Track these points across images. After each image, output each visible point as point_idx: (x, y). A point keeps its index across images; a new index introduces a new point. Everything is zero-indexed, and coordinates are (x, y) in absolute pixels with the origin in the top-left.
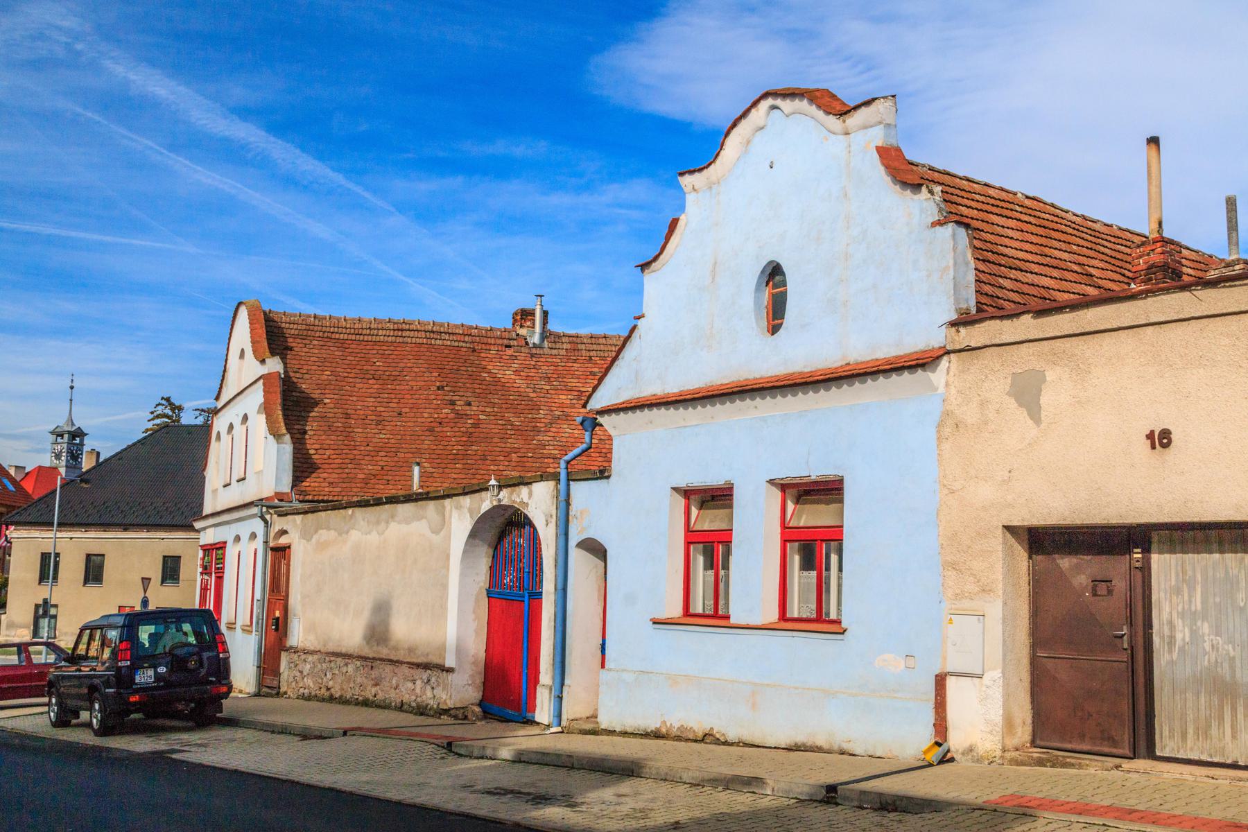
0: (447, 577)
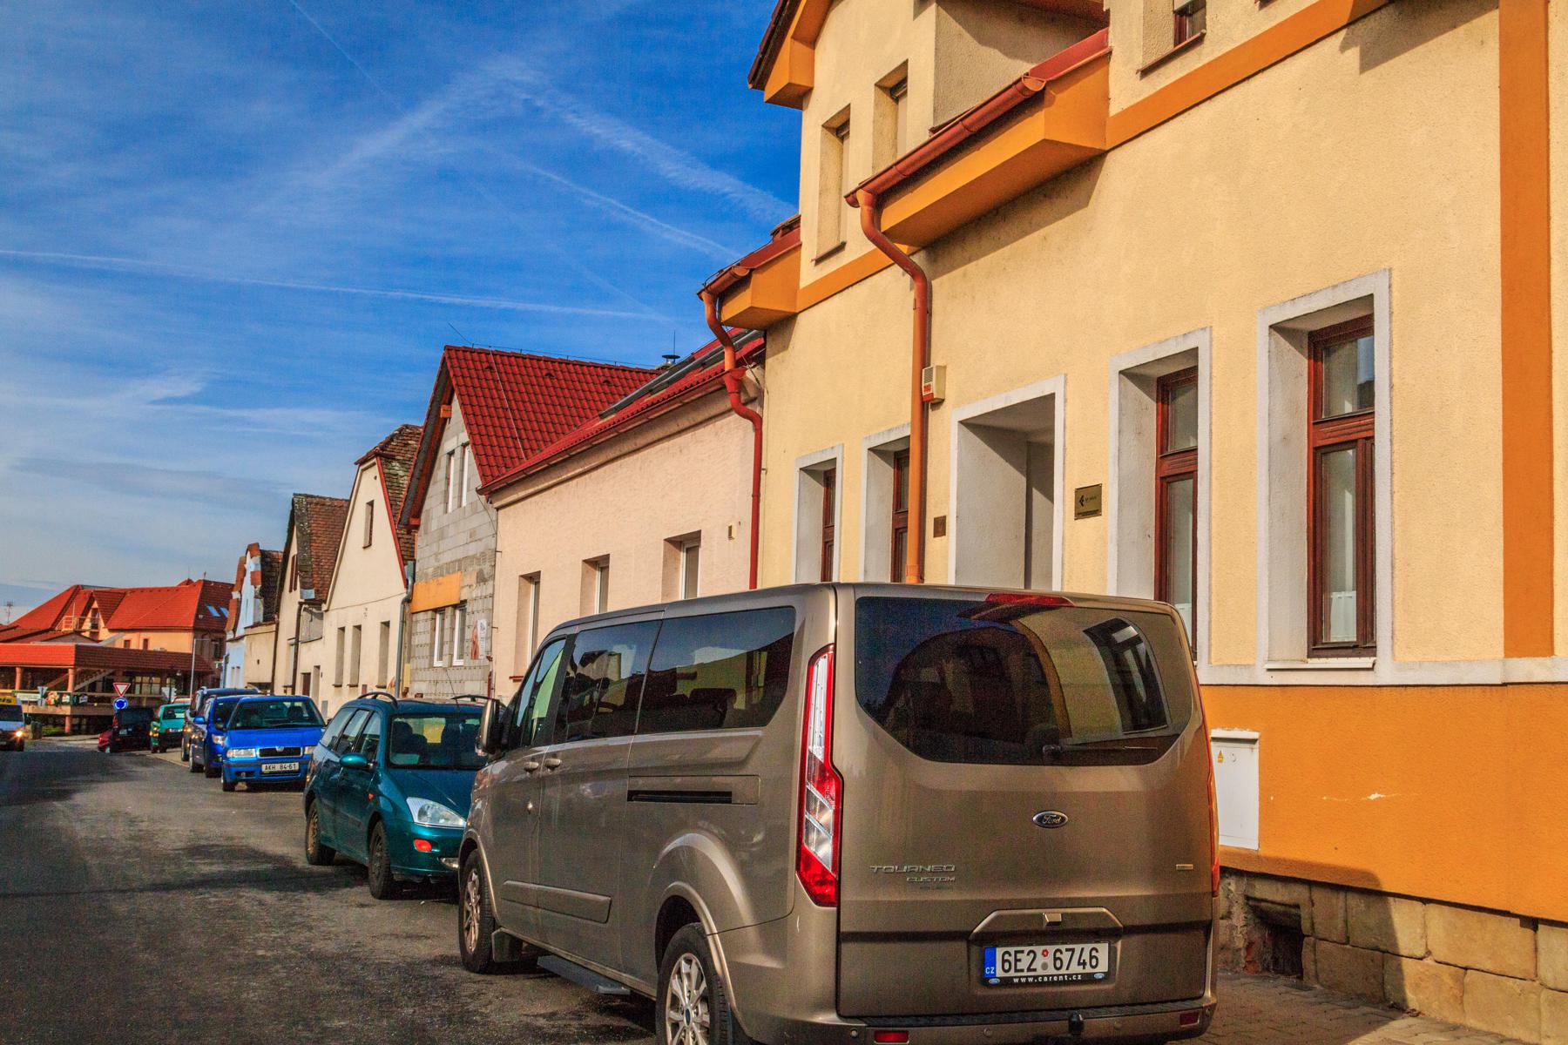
0: (1006, 916)
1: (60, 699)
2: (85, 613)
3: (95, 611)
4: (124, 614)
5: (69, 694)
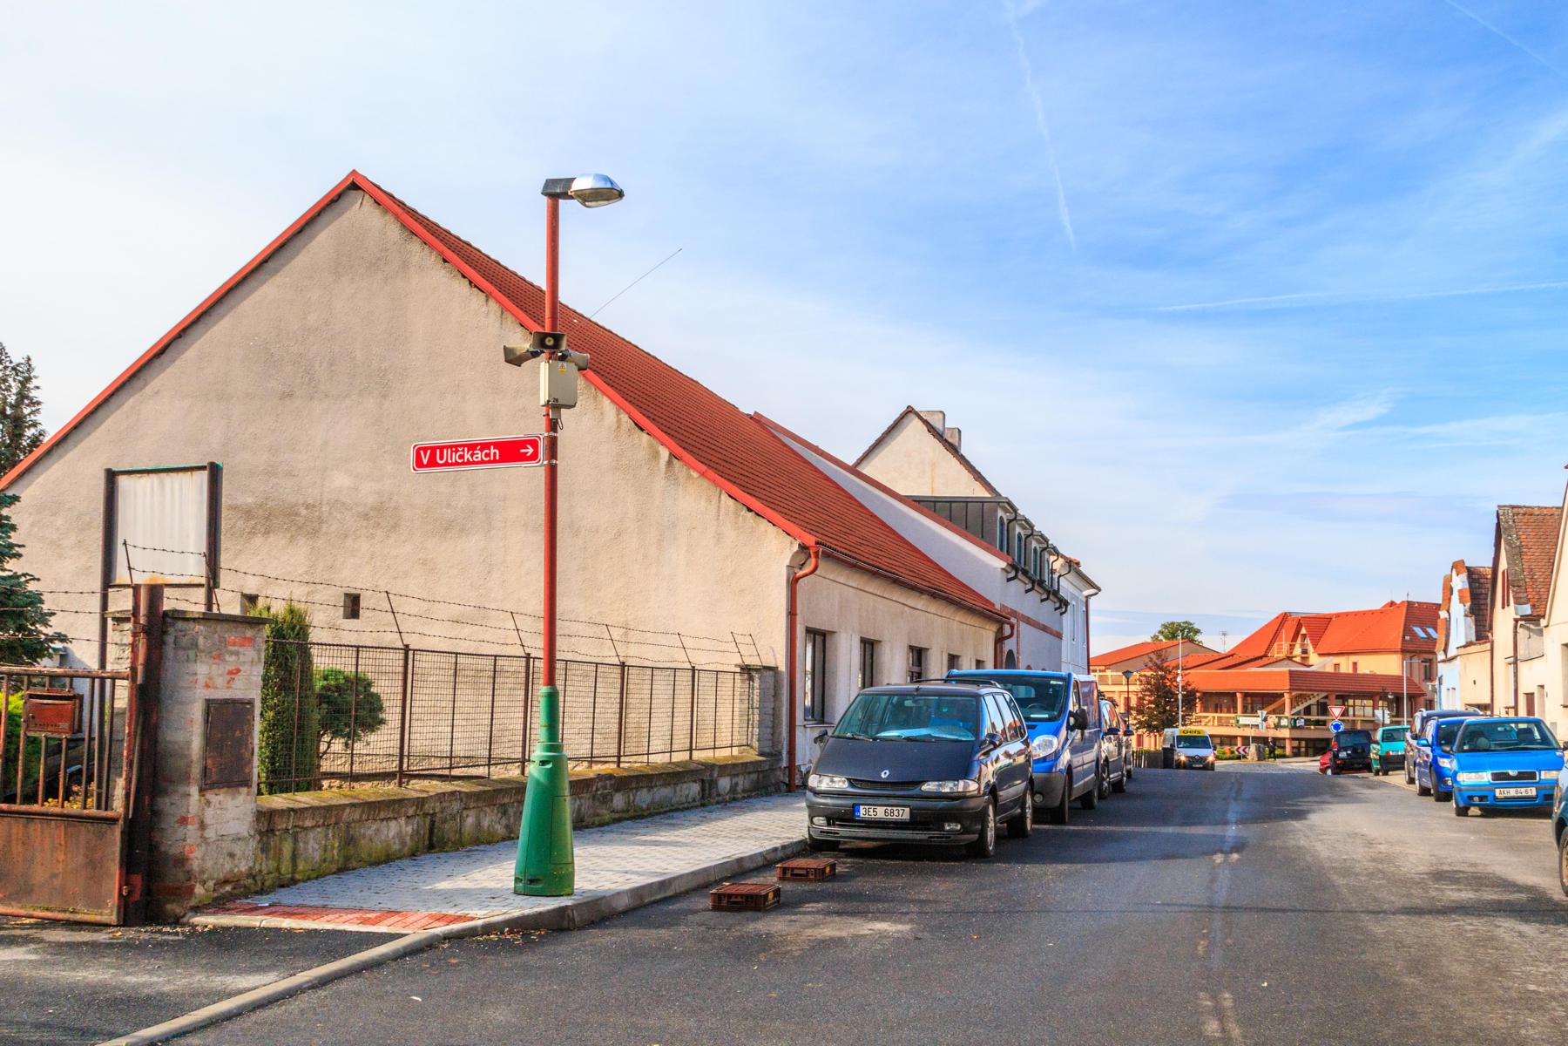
2: (1294, 639)
3: (1304, 636)
5: (1287, 718)
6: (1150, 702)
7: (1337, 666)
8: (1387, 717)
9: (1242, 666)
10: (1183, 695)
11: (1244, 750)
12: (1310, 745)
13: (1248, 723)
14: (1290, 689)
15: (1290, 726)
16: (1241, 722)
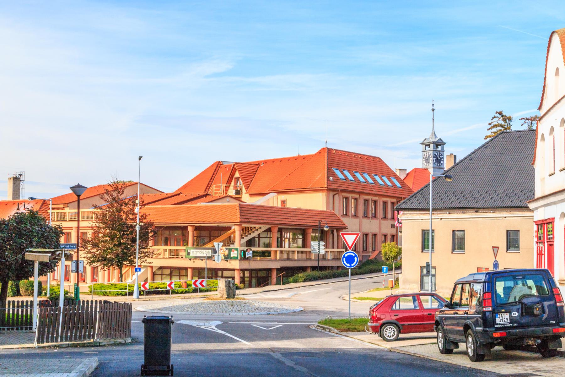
1: (229, 254)
2: (229, 182)
3: (237, 179)
4: (258, 184)
5: (237, 249)
6: (105, 235)
7: (283, 202)
8: (322, 248)
9: (193, 202)
10: (141, 226)
11: (201, 283)
12: (254, 274)
13: (198, 255)
14: (240, 222)
15: (239, 258)
16: (191, 255)
